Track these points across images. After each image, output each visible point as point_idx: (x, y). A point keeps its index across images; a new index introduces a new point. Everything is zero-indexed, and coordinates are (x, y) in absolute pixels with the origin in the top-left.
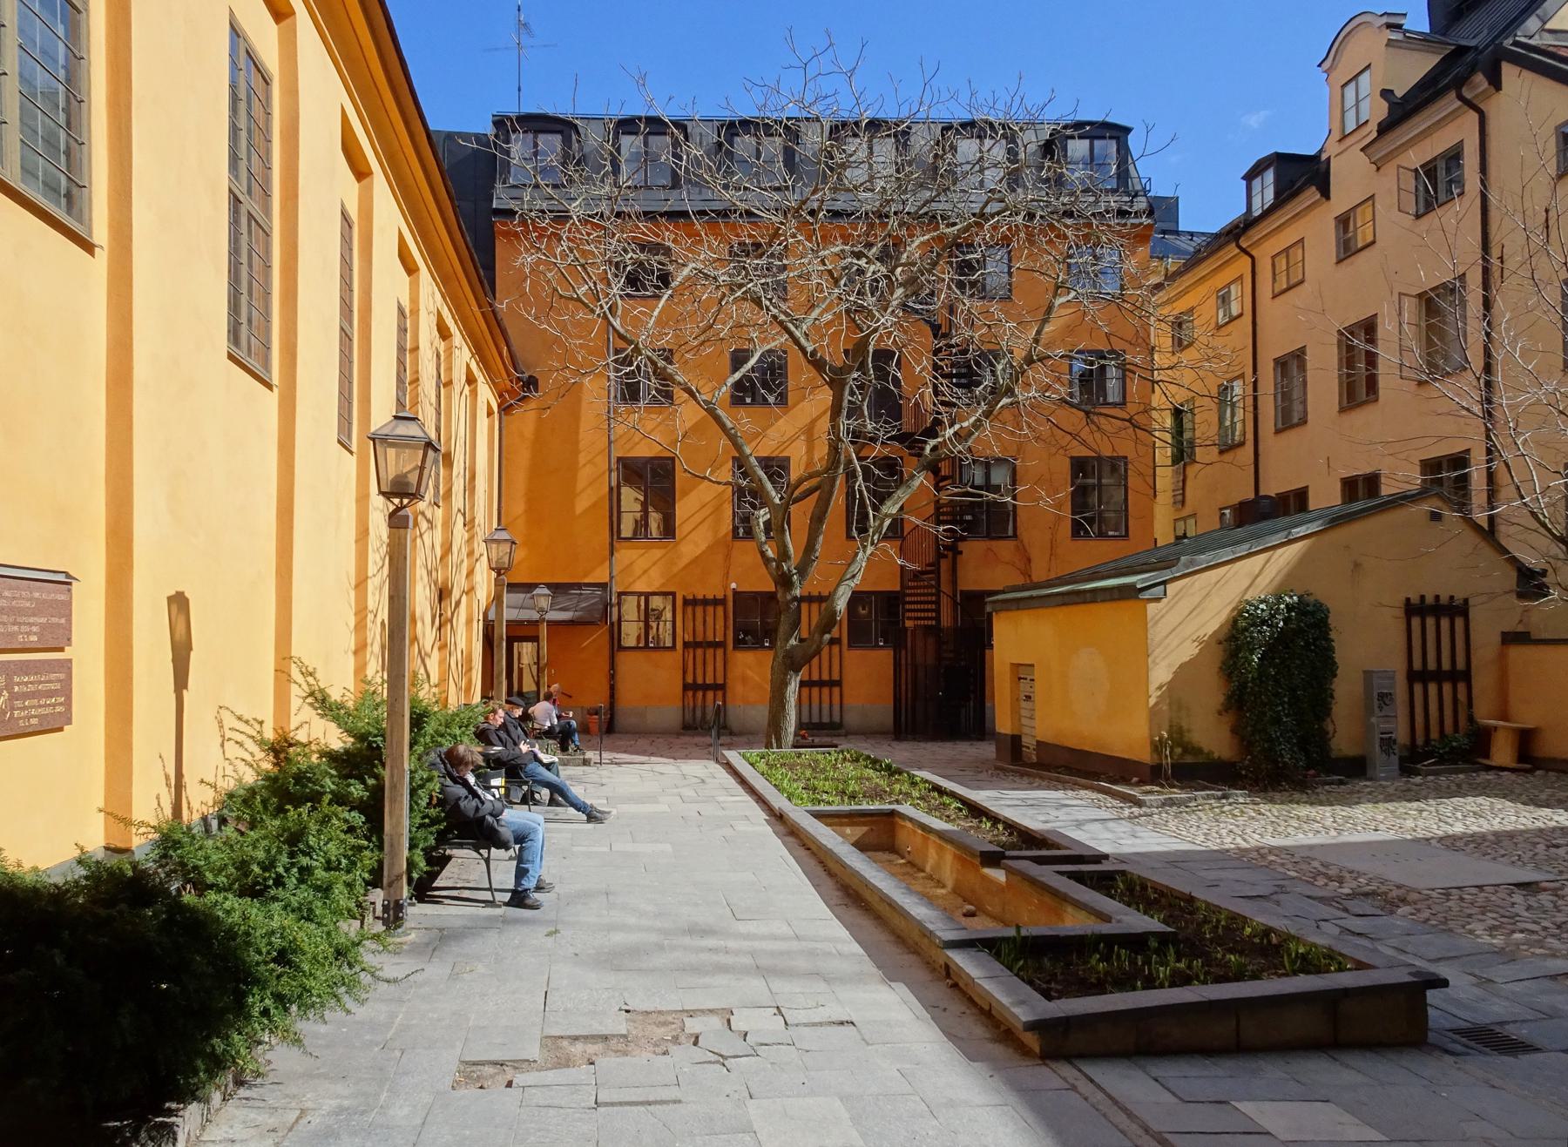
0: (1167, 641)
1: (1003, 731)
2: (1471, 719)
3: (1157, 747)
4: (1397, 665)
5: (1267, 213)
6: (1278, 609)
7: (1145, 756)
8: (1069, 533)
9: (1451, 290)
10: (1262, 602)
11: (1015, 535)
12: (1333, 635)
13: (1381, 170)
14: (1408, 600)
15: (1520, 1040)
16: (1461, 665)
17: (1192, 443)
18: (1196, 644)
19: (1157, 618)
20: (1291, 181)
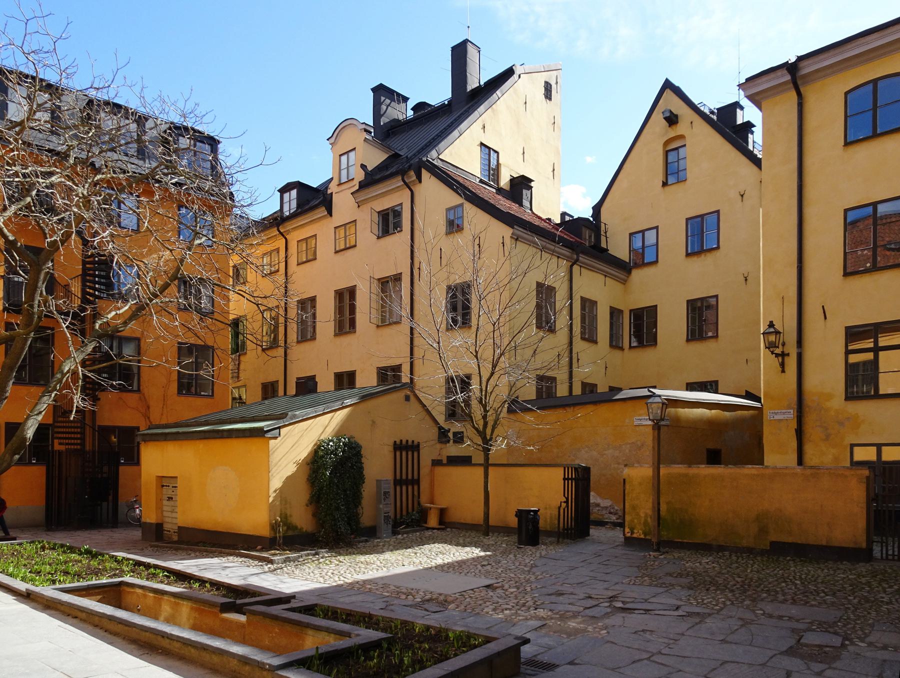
0: (280, 463)
1: (148, 521)
2: (419, 504)
3: (274, 527)
4: (390, 477)
5: (293, 216)
6: (340, 445)
7: (266, 532)
8: (176, 391)
9: (397, 278)
10: (330, 441)
11: (139, 390)
12: (363, 460)
13: (360, 208)
14: (395, 442)
15: (548, 663)
16: (416, 477)
17: (244, 343)
18: (295, 465)
19: (274, 449)
20: (308, 200)
